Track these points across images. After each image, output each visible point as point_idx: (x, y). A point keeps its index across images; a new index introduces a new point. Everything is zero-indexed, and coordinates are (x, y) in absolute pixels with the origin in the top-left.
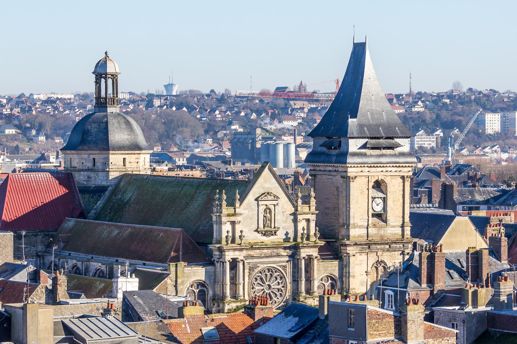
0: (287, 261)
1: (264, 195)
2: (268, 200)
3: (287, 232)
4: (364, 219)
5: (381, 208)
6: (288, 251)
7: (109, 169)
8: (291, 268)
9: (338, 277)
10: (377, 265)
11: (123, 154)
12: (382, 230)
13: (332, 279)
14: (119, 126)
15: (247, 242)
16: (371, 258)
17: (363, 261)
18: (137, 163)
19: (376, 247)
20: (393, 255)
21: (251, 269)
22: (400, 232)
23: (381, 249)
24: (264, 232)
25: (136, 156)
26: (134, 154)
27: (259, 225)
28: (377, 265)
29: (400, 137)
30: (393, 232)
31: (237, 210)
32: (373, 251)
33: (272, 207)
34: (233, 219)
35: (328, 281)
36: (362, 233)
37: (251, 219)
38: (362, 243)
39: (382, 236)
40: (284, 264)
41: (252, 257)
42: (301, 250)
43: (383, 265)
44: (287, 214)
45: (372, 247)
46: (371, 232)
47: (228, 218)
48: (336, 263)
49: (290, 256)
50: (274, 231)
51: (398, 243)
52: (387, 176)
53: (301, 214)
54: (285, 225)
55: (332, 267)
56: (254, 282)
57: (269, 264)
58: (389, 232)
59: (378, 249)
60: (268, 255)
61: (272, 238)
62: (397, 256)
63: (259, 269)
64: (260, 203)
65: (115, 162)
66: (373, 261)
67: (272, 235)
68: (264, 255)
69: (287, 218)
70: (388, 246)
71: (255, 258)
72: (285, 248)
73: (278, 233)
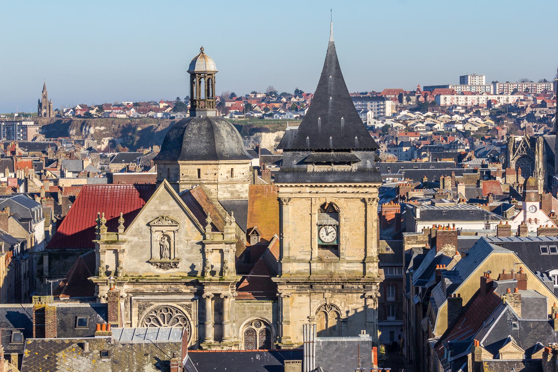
0: (191, 300)
1: (158, 219)
2: (164, 226)
3: (193, 264)
4: (306, 252)
5: (334, 235)
6: (192, 287)
7: (179, 181)
8: (197, 308)
9: (272, 322)
10: (325, 309)
11: (196, 164)
12: (332, 266)
13: (265, 324)
14: (198, 132)
15: (137, 275)
16: (316, 300)
17: (304, 303)
18: (215, 174)
19: (322, 287)
20: (350, 298)
21: (141, 309)
22: (361, 270)
23: (329, 290)
24: (159, 264)
25: (215, 166)
26: (210, 164)
27: (152, 255)
28: (325, 309)
29: (357, 150)
30: (350, 269)
31: (120, 236)
32: (317, 291)
33: (171, 235)
34: (114, 247)
35: (261, 325)
36: (303, 269)
37: (142, 247)
38: (296, 281)
39: (331, 275)
40: (188, 303)
41: (143, 293)
42: (205, 287)
43: (335, 309)
44: (192, 243)
45: (315, 287)
46: (315, 268)
47: (108, 245)
48: (269, 304)
49: (195, 294)
50: (173, 262)
51: (357, 283)
52: (339, 198)
53: (210, 244)
54: (189, 255)
55: (263, 309)
56: (147, 323)
57: (166, 302)
58: (342, 268)
59: (325, 290)
60: (163, 291)
61: (171, 270)
62: (355, 300)
63: (152, 307)
64: (154, 229)
65: (187, 173)
66: (318, 304)
67: (171, 267)
68: (158, 292)
69: (192, 248)
70: (339, 287)
71: (148, 295)
72: (187, 284)
73: (179, 265)
